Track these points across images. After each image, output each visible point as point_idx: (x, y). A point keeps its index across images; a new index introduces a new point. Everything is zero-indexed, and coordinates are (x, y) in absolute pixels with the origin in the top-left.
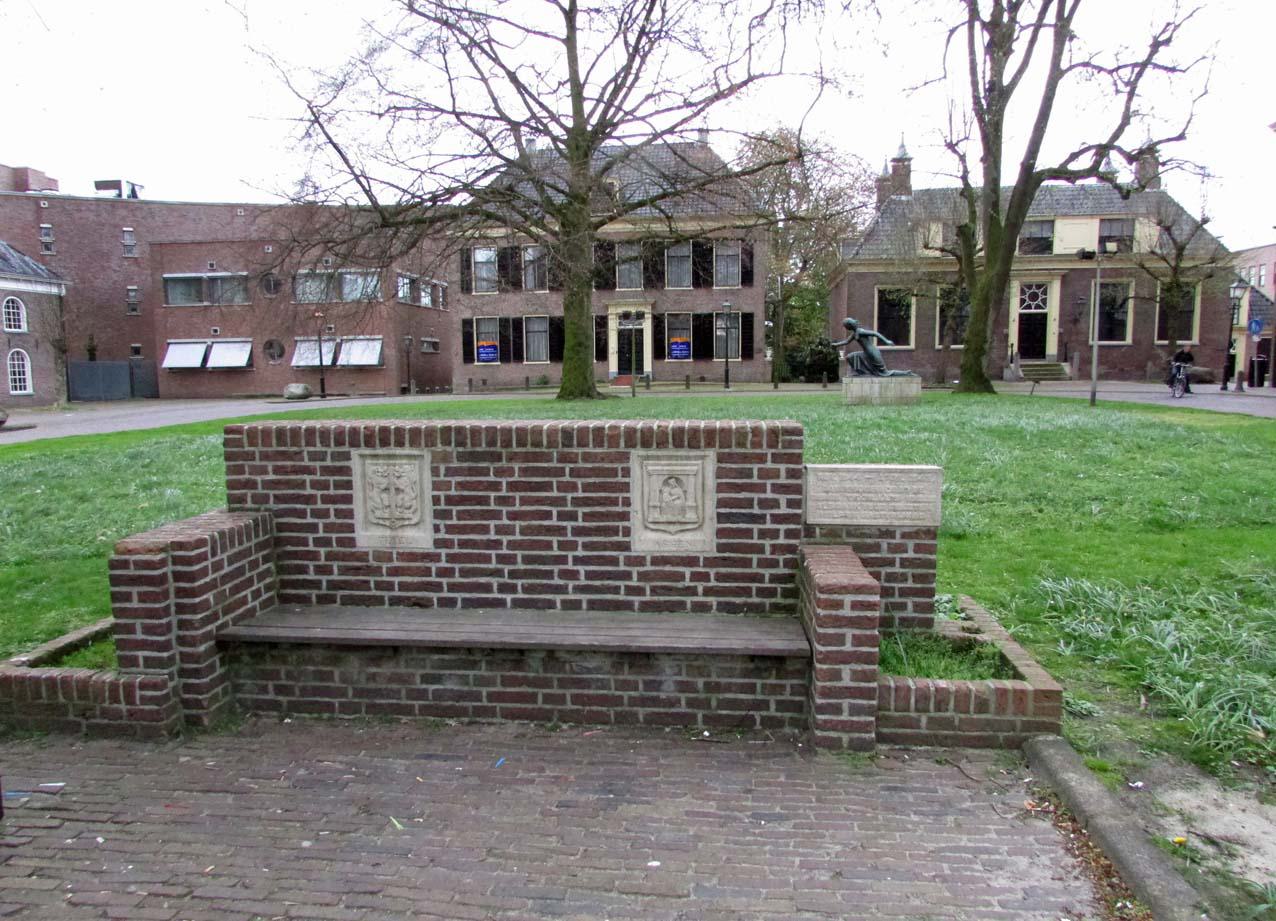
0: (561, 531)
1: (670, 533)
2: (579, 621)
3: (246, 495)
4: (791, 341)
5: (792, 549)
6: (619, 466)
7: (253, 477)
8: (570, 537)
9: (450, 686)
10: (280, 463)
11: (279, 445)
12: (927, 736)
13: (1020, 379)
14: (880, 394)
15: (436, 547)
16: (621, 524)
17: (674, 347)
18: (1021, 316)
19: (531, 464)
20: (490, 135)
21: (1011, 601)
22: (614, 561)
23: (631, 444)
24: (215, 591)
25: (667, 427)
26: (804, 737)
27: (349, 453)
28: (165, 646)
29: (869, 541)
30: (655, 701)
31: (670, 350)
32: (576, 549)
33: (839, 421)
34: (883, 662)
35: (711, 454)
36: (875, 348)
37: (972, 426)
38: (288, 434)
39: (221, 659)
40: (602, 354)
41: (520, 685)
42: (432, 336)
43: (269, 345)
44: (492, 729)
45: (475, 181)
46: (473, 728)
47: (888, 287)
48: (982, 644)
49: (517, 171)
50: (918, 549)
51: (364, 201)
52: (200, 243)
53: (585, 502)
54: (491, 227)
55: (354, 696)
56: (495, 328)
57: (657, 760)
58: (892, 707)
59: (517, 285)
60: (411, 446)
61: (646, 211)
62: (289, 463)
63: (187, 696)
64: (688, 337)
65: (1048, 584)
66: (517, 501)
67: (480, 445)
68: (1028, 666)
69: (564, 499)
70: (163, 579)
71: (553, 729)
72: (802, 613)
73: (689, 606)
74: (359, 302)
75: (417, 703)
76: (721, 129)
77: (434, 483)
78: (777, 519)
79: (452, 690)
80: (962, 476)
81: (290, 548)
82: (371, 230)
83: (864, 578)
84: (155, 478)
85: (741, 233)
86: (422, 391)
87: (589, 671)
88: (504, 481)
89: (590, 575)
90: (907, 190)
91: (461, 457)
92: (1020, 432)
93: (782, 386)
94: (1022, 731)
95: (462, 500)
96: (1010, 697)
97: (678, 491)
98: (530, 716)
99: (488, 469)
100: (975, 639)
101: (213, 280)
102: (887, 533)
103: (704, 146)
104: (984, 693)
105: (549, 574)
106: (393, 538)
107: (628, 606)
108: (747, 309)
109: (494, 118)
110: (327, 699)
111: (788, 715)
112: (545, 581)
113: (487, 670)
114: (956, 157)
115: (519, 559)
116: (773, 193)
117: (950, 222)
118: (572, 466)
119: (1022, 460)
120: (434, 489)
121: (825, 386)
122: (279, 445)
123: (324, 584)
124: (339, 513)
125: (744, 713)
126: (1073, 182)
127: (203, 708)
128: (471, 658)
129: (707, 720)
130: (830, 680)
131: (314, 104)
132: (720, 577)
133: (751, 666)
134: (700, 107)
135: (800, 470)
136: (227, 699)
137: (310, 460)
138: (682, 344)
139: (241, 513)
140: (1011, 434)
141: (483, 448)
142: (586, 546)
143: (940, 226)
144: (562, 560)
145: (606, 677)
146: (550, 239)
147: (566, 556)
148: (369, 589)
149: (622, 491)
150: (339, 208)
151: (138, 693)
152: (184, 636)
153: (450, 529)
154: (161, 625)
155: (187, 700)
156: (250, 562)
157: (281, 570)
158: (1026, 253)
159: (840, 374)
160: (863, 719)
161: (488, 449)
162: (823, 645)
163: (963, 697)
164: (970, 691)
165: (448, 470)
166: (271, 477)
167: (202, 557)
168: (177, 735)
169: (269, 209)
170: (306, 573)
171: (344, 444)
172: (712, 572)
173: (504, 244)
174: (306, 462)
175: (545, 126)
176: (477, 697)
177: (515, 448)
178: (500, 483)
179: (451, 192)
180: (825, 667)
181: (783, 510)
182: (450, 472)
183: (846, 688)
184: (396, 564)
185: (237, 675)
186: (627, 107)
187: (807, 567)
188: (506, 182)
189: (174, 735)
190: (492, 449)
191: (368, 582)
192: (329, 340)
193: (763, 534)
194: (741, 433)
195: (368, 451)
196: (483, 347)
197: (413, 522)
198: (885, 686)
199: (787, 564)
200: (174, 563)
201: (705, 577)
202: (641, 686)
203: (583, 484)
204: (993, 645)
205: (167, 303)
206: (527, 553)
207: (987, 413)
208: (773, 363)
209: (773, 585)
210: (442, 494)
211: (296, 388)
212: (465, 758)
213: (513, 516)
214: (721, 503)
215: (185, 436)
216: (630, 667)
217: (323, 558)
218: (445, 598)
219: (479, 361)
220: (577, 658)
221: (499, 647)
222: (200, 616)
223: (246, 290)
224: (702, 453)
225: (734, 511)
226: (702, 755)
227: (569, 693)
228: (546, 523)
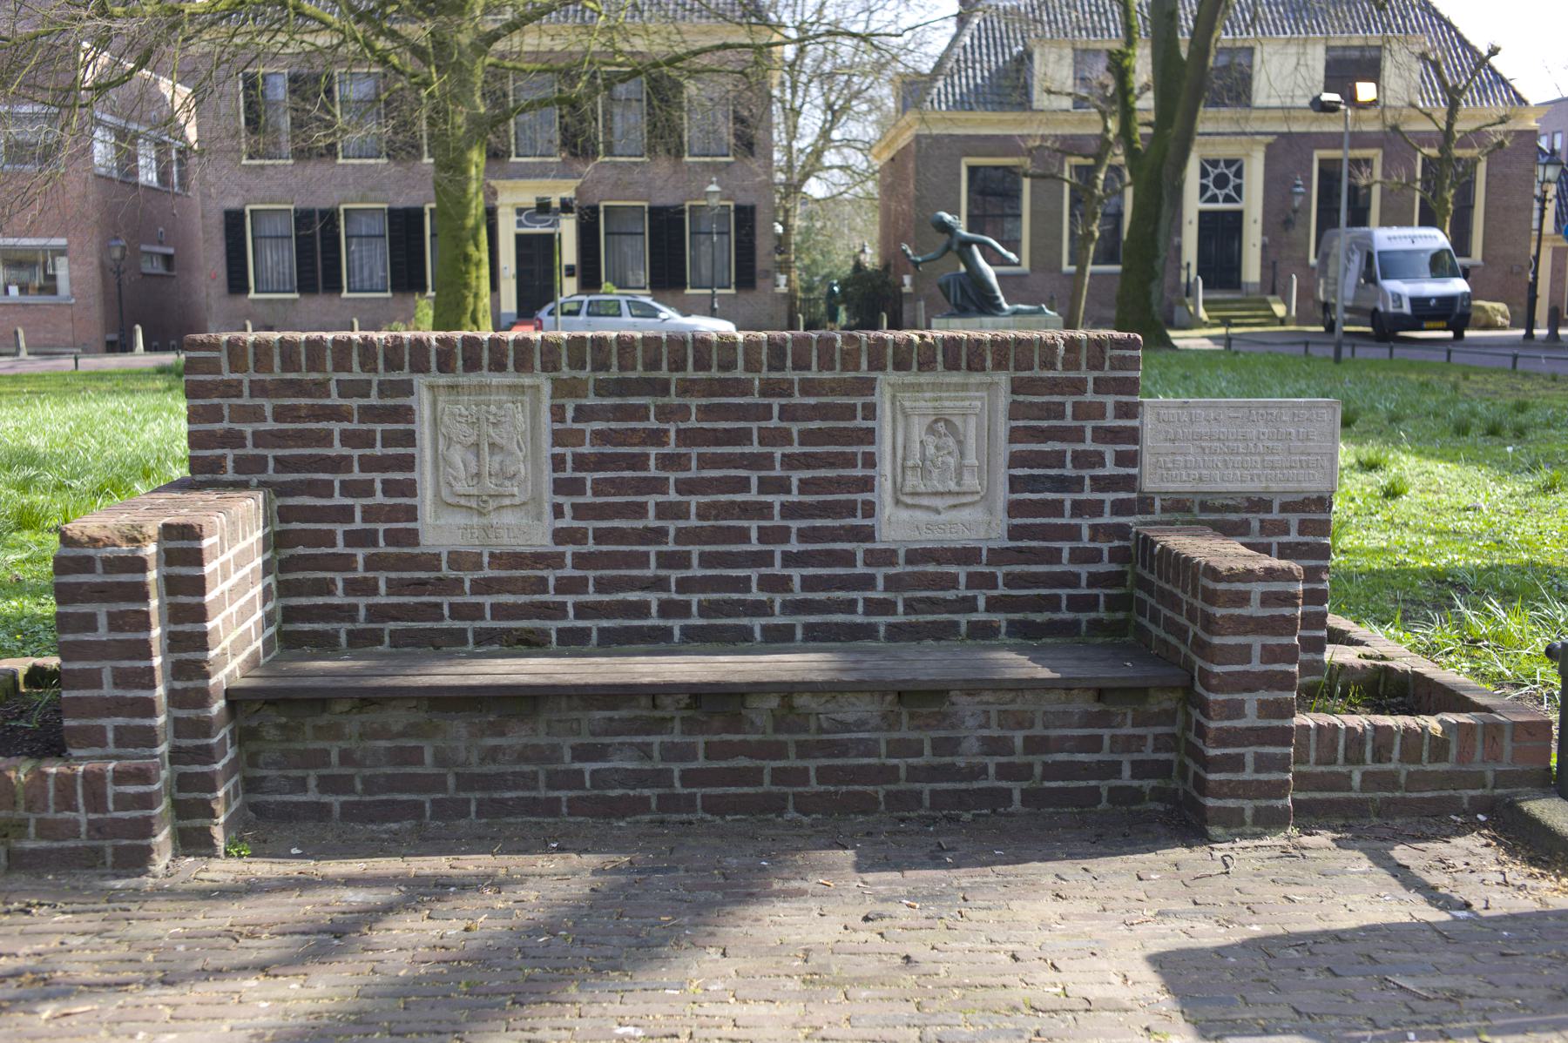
3: (224, 457)
6: (859, 401)
7: (237, 426)
11: (284, 369)
18: (1203, 215)
19: (716, 400)
22: (848, 559)
23: (877, 364)
27: (410, 383)
29: (1233, 517)
35: (1003, 379)
42: (161, 243)
55: (458, 788)
60: (517, 369)
67: (634, 368)
73: (963, 628)
77: (555, 433)
78: (1101, 484)
81: (301, 550)
88: (672, 428)
89: (809, 584)
91: (602, 389)
95: (601, 462)
106: (485, 529)
111: (1148, 784)
113: (683, 733)
115: (695, 561)
118: (784, 401)
120: (555, 443)
122: (284, 369)
123: (362, 612)
124: (390, 488)
132: (1011, 581)
141: (638, 373)
142: (804, 536)
144: (764, 559)
145: (874, 735)
149: (861, 442)
151: (111, 790)
153: (580, 512)
165: (579, 410)
166: (270, 425)
170: (331, 593)
172: (1000, 572)
174: (335, 400)
177: (691, 373)
181: (1110, 469)
182: (582, 414)
184: (488, 573)
191: (439, 606)
193: (1079, 508)
195: (443, 380)
197: (517, 501)
206: (707, 548)
210: (568, 452)
213: (686, 487)
214: (1015, 460)
217: (360, 565)
218: (570, 630)
225: (1036, 472)
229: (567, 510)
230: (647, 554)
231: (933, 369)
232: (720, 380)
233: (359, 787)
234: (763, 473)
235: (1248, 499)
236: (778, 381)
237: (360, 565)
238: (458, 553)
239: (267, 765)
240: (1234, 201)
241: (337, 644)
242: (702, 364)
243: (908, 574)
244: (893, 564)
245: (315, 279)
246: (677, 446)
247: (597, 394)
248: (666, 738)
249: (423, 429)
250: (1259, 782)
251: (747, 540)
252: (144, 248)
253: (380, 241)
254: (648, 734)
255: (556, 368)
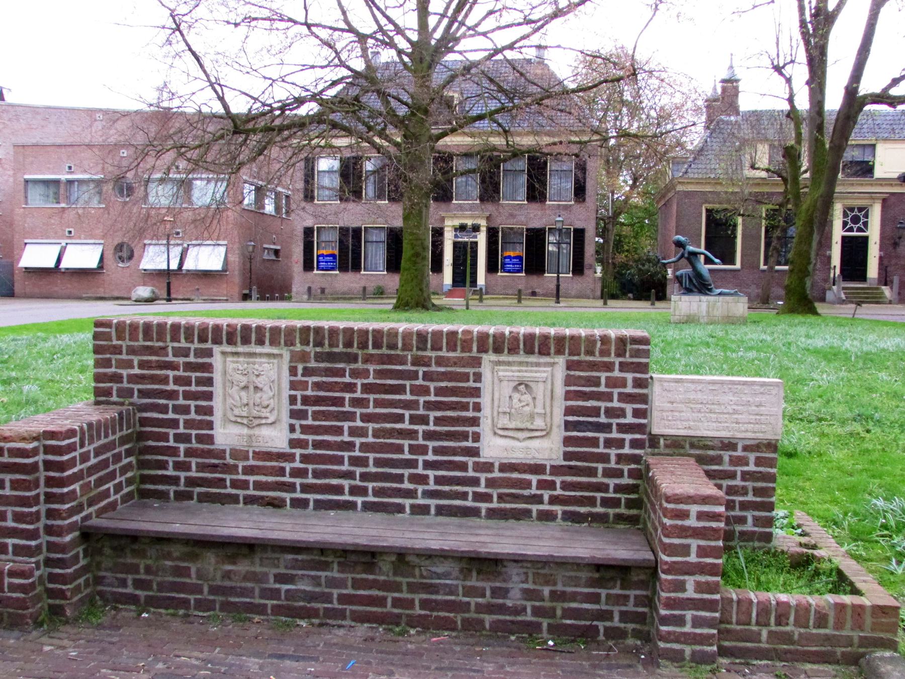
0: (412, 434)
1: (518, 439)
2: (429, 526)
3: (111, 388)
4: (621, 258)
5: (636, 459)
6: (471, 371)
7: (120, 371)
8: (421, 441)
9: (304, 586)
10: (145, 358)
12: (768, 650)
13: (842, 302)
14: (708, 312)
15: (291, 448)
16: (471, 429)
17: (507, 260)
18: (844, 238)
20: (339, 46)
21: (844, 519)
22: (463, 467)
23: (483, 349)
24: (81, 482)
25: (518, 333)
26: (647, 649)
27: (211, 350)
28: (33, 535)
29: (711, 453)
30: (502, 609)
31: (503, 264)
32: (426, 453)
33: (669, 339)
34: (724, 575)
35: (561, 361)
36: (704, 268)
37: (798, 346)
38: (155, 329)
39: (85, 551)
40: (438, 267)
41: (370, 588)
42: (274, 244)
43: (119, 247)
44: (341, 632)
45: (323, 91)
46: (324, 630)
47: (717, 206)
48: (819, 560)
49: (362, 82)
50: (759, 462)
51: (218, 108)
52: (60, 146)
53: (437, 406)
54: (336, 137)
56: (334, 237)
57: (503, 667)
58: (734, 620)
59: (357, 194)
61: (485, 124)
62: (154, 358)
63: (51, 586)
64: (520, 251)
65: (880, 503)
66: (371, 404)
67: (338, 346)
68: (865, 581)
69: (416, 402)
70: (34, 467)
71: (401, 634)
72: (645, 523)
73: (534, 514)
74: (208, 207)
75: (270, 603)
76: (559, 46)
77: (291, 382)
78: (623, 428)
79: (305, 591)
80: (790, 395)
81: (151, 443)
82: (222, 137)
83: (709, 489)
84: (14, 374)
85: (575, 149)
86: (262, 298)
87: (439, 576)
88: (359, 382)
89: (439, 480)
90: (737, 113)
91: (319, 357)
92: (845, 353)
93: (611, 303)
94: (860, 646)
95: (318, 401)
96: (849, 612)
97: (527, 398)
98: (380, 619)
99: (344, 370)
100: (813, 555)
101: (70, 182)
102: (729, 445)
103: (541, 61)
104: (824, 608)
105: (399, 478)
106: (250, 436)
107: (475, 512)
108: (579, 225)
109: (343, 30)
110: (182, 596)
111: (630, 626)
112: (395, 485)
113: (339, 571)
114: (783, 80)
115: (371, 462)
116: (606, 111)
117: (776, 143)
118: (425, 369)
119: (849, 381)
121: (653, 304)
123: (183, 480)
125: (588, 623)
126: (894, 107)
127: (65, 598)
128: (323, 559)
129: (552, 629)
130: (673, 591)
131: (175, 13)
132: (566, 486)
133: (597, 575)
134: (539, 24)
135: (647, 379)
136: (88, 590)
137: (174, 356)
138: (515, 258)
139: (106, 407)
140: (835, 355)
141: (340, 349)
142: (436, 451)
143: (767, 147)
144: (412, 464)
145: (455, 582)
146: (392, 150)
147: (417, 460)
148: (225, 487)
149: (472, 396)
150: (194, 114)
152: (53, 525)
153: (305, 429)
154: (31, 513)
155: (52, 589)
156: (114, 456)
157: (142, 464)
158: (848, 175)
159: (668, 291)
160: (705, 631)
161: (344, 350)
162: (668, 556)
163: (803, 611)
164: (810, 605)
166: (136, 371)
167: (71, 448)
168: (41, 625)
169: (126, 114)
170: (166, 469)
171: (206, 341)
172: (558, 480)
173: (348, 154)
174: (170, 358)
175: (391, 38)
176: (327, 598)
177: (371, 350)
178: (355, 384)
179: (300, 101)
180: (670, 577)
181: (629, 419)
182: (307, 372)
183: (688, 599)
184: (252, 462)
185: (98, 566)
186: (470, 22)
187: (653, 476)
188: (354, 92)
189: (38, 624)
190: (349, 350)
191: (224, 480)
192: (178, 245)
193: (609, 443)
194: (590, 341)
196: (322, 255)
197: (269, 421)
198: (728, 598)
199: (632, 474)
200: (46, 453)
201: (551, 485)
202: (488, 593)
203: (435, 388)
204: (830, 561)
205: (26, 204)
207: (812, 332)
208: (603, 279)
209: (618, 496)
210: (299, 394)
211: (144, 291)
212: (316, 659)
213: (366, 418)
214: (569, 411)
215: (39, 334)
216: (478, 573)
217: (182, 454)
219: (318, 269)
220: (428, 562)
221: (351, 548)
222: (67, 506)
223: (100, 193)
224: (552, 360)
225: (581, 419)
226: (546, 664)
227: (417, 597)
228: (398, 426)
229: (297, 427)
230: (343, 457)
231: (518, 353)
232: (388, 355)
233: (155, 587)
234: (412, 412)
235: (722, 442)
236: (423, 357)
237: (182, 454)
238: (236, 450)
239: (106, 570)
240: (864, 231)
241: (169, 498)
242: (377, 345)
243: (500, 478)
244: (491, 471)
245: (348, 263)
246: (362, 393)
247: (316, 361)
248: (328, 574)
249: (217, 377)
250: (695, 634)
251: (402, 452)
252: (266, 246)
253: (381, 245)
254: (318, 570)
255: (293, 344)
